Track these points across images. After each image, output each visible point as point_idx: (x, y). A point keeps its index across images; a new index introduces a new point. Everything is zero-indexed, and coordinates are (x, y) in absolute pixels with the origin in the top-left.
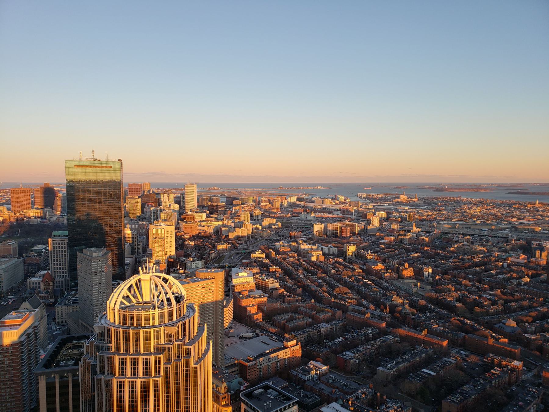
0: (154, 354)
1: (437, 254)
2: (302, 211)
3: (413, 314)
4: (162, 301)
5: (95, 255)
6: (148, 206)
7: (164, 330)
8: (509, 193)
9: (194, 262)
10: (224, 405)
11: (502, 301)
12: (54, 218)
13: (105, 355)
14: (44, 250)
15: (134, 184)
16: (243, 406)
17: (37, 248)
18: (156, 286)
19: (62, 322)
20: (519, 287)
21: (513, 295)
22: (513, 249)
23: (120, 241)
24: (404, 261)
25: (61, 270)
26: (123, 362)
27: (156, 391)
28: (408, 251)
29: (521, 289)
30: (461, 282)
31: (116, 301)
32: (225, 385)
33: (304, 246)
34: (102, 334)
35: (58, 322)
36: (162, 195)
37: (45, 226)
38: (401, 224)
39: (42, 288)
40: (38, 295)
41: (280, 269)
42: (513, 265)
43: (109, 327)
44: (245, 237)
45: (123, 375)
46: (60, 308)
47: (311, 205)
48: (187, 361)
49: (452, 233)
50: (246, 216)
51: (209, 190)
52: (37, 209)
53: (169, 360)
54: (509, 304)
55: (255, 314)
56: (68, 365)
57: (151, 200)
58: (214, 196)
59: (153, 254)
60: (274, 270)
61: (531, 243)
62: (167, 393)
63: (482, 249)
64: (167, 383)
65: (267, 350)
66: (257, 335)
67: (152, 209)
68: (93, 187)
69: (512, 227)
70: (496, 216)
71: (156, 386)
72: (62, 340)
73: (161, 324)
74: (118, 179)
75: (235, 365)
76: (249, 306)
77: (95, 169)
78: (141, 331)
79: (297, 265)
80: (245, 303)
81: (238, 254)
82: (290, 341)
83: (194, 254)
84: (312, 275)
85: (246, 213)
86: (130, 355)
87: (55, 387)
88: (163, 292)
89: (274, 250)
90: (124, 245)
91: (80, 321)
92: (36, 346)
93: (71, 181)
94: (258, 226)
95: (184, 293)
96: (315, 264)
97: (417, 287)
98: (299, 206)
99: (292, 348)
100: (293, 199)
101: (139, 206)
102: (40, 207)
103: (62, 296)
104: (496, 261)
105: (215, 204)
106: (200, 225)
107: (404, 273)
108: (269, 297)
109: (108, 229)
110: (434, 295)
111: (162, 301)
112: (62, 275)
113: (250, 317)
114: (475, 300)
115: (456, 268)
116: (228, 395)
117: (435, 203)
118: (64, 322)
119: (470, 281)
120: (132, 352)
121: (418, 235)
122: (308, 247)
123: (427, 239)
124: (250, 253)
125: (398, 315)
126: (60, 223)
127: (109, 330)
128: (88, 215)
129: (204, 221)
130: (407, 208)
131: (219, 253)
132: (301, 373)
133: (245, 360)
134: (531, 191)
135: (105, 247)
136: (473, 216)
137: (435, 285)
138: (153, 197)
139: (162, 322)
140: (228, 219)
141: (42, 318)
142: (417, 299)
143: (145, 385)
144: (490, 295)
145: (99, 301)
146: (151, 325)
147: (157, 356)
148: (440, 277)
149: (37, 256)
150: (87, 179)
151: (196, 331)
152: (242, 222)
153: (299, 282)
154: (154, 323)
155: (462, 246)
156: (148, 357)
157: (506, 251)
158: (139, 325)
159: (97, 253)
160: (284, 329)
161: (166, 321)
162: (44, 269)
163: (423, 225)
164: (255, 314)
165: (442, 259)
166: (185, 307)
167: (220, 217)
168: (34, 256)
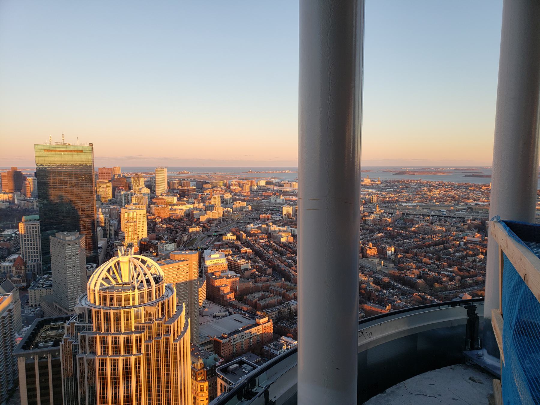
0: (135, 333)
1: (399, 234)
2: (272, 194)
3: (378, 291)
4: (142, 282)
5: (68, 238)
6: (118, 190)
7: (145, 309)
8: (466, 176)
9: (167, 245)
10: (200, 380)
11: (459, 277)
12: (23, 203)
13: (86, 335)
14: (14, 235)
15: (104, 168)
16: (219, 381)
17: (6, 233)
18: (135, 268)
19: (36, 305)
20: (474, 263)
21: (469, 271)
22: (469, 229)
23: (94, 224)
24: (368, 241)
25: (33, 255)
26: (104, 342)
27: (138, 367)
28: (372, 231)
29: (476, 265)
30: (422, 260)
31: (96, 283)
32: (201, 361)
33: (274, 228)
34: (81, 316)
35: (32, 306)
36: (132, 179)
37: (13, 210)
38: (365, 206)
39: (14, 272)
40: (10, 279)
41: (251, 251)
42: (469, 243)
43: (89, 307)
44: (216, 219)
45: (104, 354)
46: (33, 291)
47: (280, 188)
48: (167, 339)
49: (412, 214)
50: (217, 199)
51: (179, 174)
52: (4, 193)
53: (149, 338)
54: (466, 279)
55: (228, 293)
56: (47, 347)
57: (121, 184)
58: (184, 180)
59: (126, 237)
60: (245, 251)
61: (485, 222)
62: (148, 369)
63: (441, 228)
64: (148, 360)
65: (240, 327)
66: (231, 314)
67: (122, 193)
68: (64, 172)
69: (469, 208)
70: (454, 198)
71: (138, 363)
72: (39, 322)
73: (141, 303)
74: (89, 163)
75: (209, 343)
76: (222, 286)
77: (66, 153)
78: (122, 311)
79: (268, 246)
80: (218, 283)
81: (209, 236)
82: (262, 318)
83: (166, 237)
84: (281, 256)
85: (217, 196)
86: (111, 334)
87: (48, 366)
88: (142, 273)
89: (245, 232)
90: (97, 228)
91: (55, 304)
92: (11, 329)
93: (41, 165)
94: (229, 209)
95: (162, 274)
96: (284, 245)
97: (380, 265)
98: (268, 189)
99: (264, 325)
100: (263, 183)
101: (110, 190)
102: (7, 191)
103: (35, 280)
104: (454, 240)
105: (185, 188)
106: (171, 209)
107: (369, 252)
108: (241, 277)
109: (80, 213)
110: (396, 272)
111: (142, 282)
112: (33, 259)
113: (223, 296)
114: (434, 277)
115: (417, 247)
116: (204, 371)
117: (396, 186)
118: (38, 305)
119: (430, 259)
120: (113, 331)
121: (381, 217)
122: (278, 229)
123: (390, 220)
124: (221, 235)
125: (363, 292)
126: (30, 208)
127: (90, 311)
128: (61, 197)
129: (175, 205)
130: (370, 191)
131: (191, 236)
132: (274, 349)
133: (219, 338)
134: (485, 174)
135: (79, 230)
136: (432, 198)
137: (398, 263)
138: (123, 181)
139: (141, 302)
140: (198, 202)
141: (15, 302)
142: (381, 277)
143: (127, 362)
144: (448, 271)
145: (73, 284)
146: (131, 305)
147: (138, 335)
148: (402, 256)
149: (7, 241)
150: (58, 163)
151: (175, 310)
152: (213, 206)
153: (269, 262)
154: (134, 303)
155: (423, 227)
156: (129, 335)
157: (462, 231)
158: (120, 305)
159: (70, 237)
160: (256, 307)
161: (146, 301)
162: (15, 253)
163: (386, 207)
164: (228, 293)
165: (404, 239)
166: (164, 287)
167: (191, 200)
168: (4, 240)
